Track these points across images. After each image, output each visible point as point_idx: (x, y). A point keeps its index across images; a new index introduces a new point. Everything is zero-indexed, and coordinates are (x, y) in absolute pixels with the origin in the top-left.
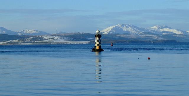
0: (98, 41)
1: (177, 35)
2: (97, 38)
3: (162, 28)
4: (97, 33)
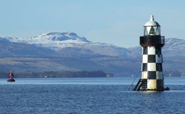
0: (152, 59)
1: (105, 59)
2: (151, 50)
3: (63, 37)
4: (149, 29)
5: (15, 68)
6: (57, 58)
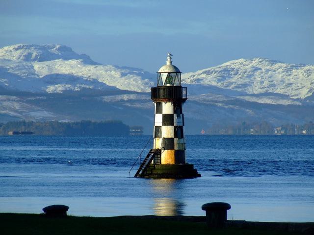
0: (168, 120)
1: (125, 97)
2: (167, 108)
3: (46, 56)
4: (164, 77)
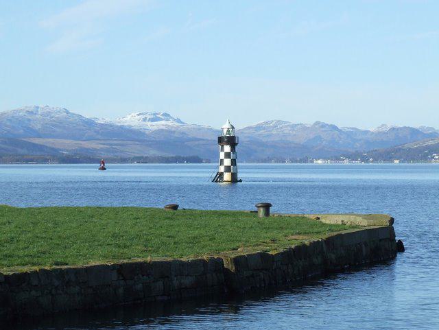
0: (228, 155)
1: (201, 142)
2: (227, 148)
3: (155, 119)
4: (225, 131)
5: (102, 153)
6: (149, 141)
